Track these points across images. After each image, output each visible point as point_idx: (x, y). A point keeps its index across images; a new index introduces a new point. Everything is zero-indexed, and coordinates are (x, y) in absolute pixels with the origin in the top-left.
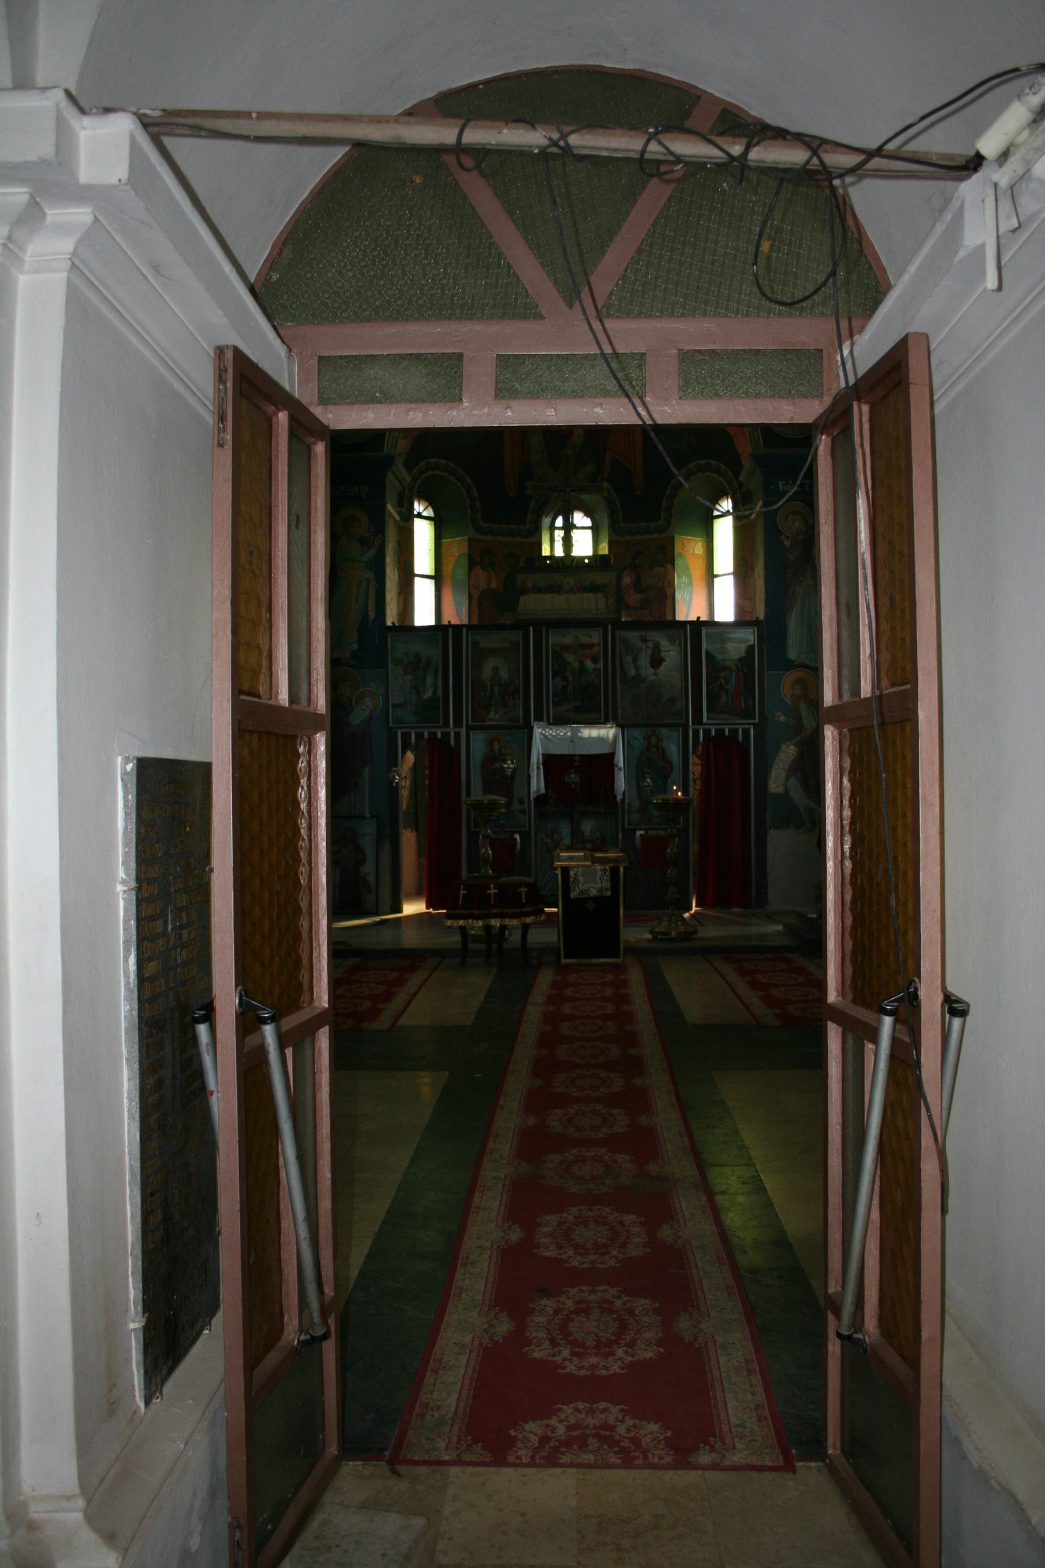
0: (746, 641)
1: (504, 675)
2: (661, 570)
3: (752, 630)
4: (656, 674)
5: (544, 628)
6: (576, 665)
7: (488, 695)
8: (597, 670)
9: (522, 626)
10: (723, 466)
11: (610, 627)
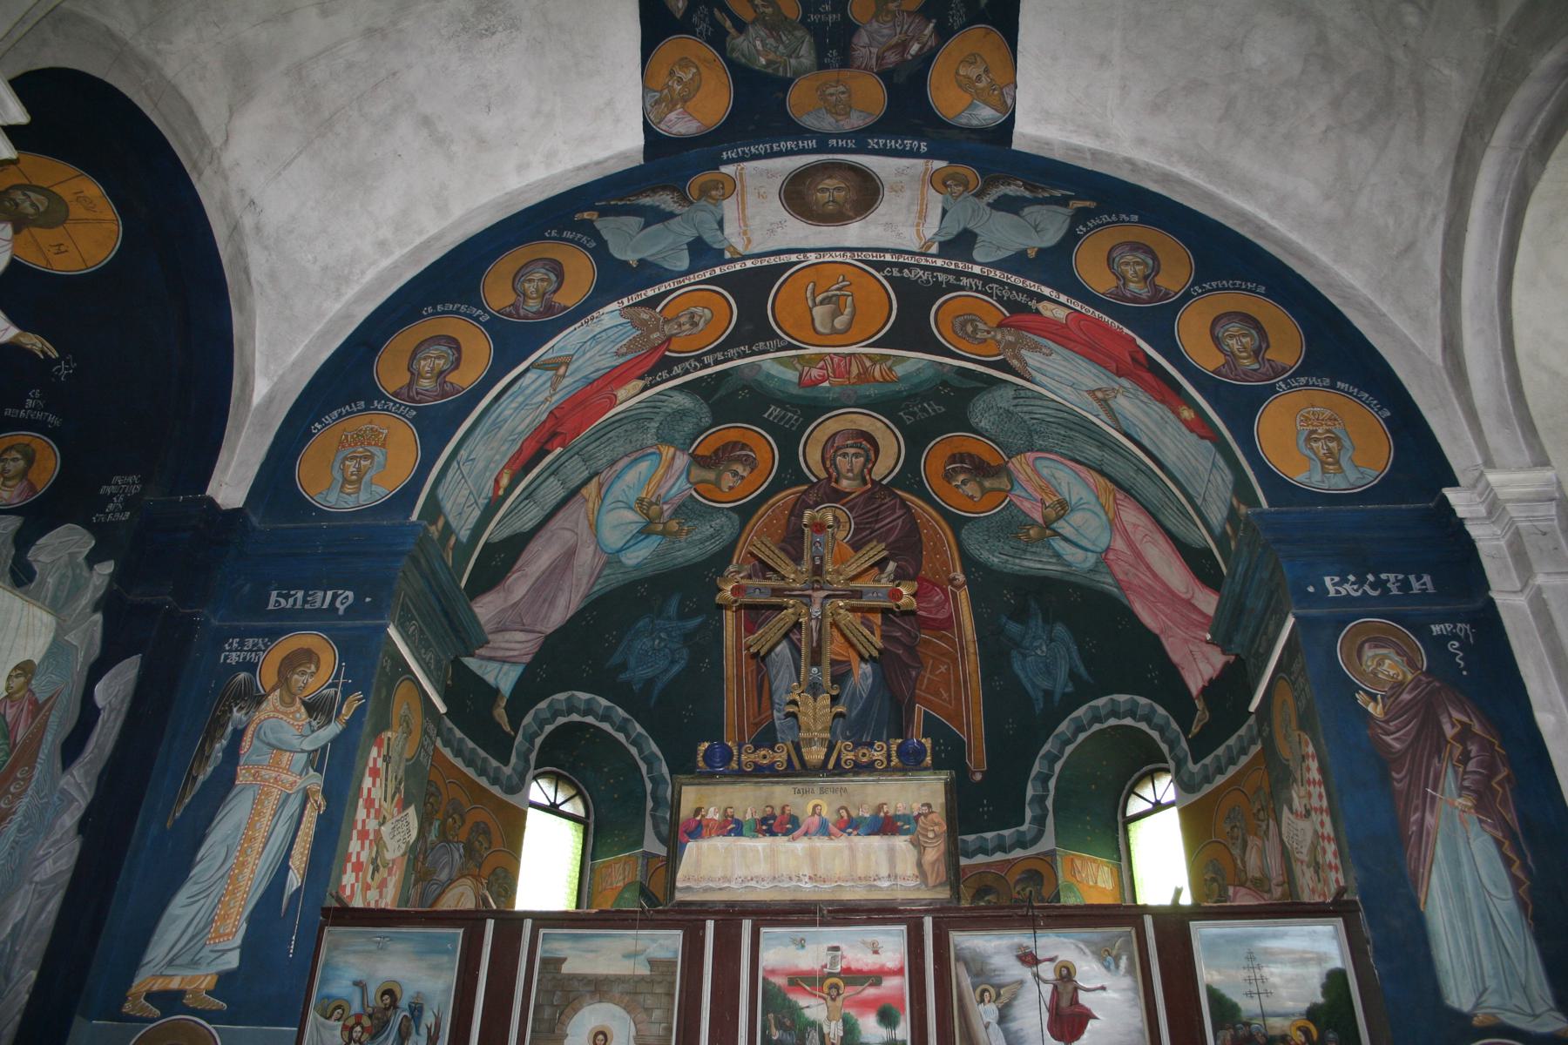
0: (1320, 959)
3: (1330, 928)
5: (747, 924)
6: (835, 1030)
9: (689, 918)
11: (928, 922)
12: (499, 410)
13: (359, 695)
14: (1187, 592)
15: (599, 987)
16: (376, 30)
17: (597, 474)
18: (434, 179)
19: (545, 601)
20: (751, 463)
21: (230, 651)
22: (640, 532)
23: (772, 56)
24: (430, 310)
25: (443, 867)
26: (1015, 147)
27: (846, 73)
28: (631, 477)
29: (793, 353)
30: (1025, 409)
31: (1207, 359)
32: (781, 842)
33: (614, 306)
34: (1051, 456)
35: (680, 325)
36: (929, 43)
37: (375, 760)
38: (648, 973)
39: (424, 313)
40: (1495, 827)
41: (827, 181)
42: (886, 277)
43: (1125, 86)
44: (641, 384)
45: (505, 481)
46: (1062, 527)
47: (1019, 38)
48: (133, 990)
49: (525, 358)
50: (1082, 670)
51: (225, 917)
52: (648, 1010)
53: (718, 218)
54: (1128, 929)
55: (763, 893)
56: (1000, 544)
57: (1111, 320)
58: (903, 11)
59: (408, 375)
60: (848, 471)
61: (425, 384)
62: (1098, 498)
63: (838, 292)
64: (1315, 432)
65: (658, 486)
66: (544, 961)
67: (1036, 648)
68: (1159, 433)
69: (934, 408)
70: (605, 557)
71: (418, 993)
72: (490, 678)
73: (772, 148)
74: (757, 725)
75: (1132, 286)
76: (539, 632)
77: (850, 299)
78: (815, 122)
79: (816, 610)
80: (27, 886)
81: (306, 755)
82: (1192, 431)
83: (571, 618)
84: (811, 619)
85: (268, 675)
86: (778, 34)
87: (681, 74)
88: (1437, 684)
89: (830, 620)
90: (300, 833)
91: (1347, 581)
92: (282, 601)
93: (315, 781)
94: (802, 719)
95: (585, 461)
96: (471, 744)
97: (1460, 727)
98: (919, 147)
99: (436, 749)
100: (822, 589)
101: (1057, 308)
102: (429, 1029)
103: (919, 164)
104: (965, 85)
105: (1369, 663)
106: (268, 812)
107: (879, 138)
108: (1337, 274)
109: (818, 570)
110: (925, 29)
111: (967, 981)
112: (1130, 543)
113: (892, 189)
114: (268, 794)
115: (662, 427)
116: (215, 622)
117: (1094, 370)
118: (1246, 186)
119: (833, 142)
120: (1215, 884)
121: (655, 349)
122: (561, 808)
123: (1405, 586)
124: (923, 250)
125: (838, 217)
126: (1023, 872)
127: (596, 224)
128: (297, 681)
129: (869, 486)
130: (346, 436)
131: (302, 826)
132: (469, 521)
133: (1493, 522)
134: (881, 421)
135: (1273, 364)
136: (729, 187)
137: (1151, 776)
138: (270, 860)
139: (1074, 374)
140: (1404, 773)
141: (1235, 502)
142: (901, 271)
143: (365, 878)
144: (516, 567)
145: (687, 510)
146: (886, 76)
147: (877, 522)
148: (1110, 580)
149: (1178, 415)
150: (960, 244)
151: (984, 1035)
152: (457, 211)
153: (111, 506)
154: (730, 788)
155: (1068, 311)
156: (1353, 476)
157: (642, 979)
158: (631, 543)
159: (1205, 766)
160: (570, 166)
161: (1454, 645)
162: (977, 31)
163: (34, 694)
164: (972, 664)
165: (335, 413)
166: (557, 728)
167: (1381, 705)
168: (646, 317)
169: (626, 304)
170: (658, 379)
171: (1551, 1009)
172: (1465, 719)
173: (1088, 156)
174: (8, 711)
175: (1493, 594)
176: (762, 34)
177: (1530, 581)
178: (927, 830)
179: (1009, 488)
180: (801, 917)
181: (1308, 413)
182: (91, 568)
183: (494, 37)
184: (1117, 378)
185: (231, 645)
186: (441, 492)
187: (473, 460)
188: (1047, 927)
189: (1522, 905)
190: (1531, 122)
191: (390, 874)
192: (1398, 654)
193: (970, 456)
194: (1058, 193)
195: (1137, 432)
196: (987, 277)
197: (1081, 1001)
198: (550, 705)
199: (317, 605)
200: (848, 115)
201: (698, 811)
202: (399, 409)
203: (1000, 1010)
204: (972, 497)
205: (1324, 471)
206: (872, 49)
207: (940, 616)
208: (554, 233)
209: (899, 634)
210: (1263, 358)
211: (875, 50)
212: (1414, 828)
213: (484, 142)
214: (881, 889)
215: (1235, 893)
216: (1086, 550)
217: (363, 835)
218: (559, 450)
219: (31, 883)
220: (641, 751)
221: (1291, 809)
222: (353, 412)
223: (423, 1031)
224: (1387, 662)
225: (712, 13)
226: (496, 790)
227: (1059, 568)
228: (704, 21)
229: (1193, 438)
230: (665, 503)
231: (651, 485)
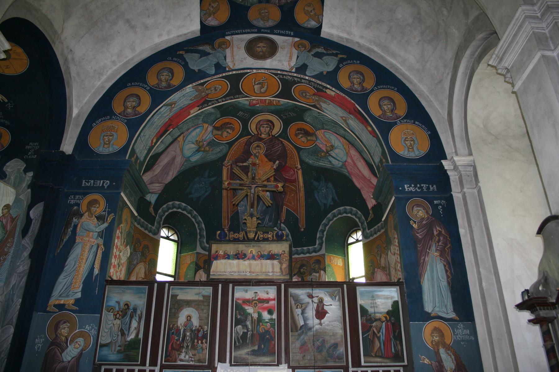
0: (392, 298)
1: (196, 322)
2: (317, 275)
3: (395, 289)
4: (321, 324)
5: (231, 285)
6: (255, 316)
7: (181, 339)
8: (271, 319)
9: (213, 283)
10: (354, 209)
11: (283, 285)
13: (113, 214)
14: (369, 177)
15: (188, 303)
17: (183, 133)
19: (165, 173)
20: (233, 129)
22: (196, 151)
24: (130, 84)
25: (135, 260)
26: (322, 36)
28: (194, 134)
29: (248, 98)
30: (321, 117)
31: (376, 112)
32: (241, 261)
33: (190, 86)
34: (329, 132)
35: (211, 91)
37: (118, 234)
38: (202, 299)
40: (444, 261)
41: (260, 44)
42: (278, 78)
44: (198, 108)
45: (155, 141)
46: (332, 153)
48: (49, 304)
49: (162, 103)
50: (336, 198)
51: (76, 283)
52: (203, 310)
53: (224, 55)
54: (339, 288)
55: (236, 276)
60: (264, 132)
61: (129, 111)
62: (343, 146)
64: (407, 138)
65: (203, 136)
66: (172, 296)
67: (323, 190)
69: (292, 114)
70: (185, 159)
71: (135, 305)
73: (242, 31)
74: (233, 211)
76: (164, 183)
77: (266, 83)
78: (257, 23)
79: (253, 191)
80: (15, 274)
81: (97, 233)
82: (371, 134)
84: (251, 194)
85: (84, 207)
87: (213, 5)
88: (434, 219)
89: (257, 194)
90: (97, 257)
93: (101, 241)
94: (248, 225)
95: (179, 129)
96: (142, 220)
97: (438, 232)
98: (291, 33)
99: (135, 226)
100: (254, 184)
101: (332, 92)
102: (139, 315)
103: (290, 39)
105: (415, 212)
106: (87, 251)
107: (278, 30)
108: (419, 87)
109: (253, 178)
111: (293, 302)
113: (281, 48)
114: (86, 245)
116: (66, 190)
118: (394, 55)
119: (263, 30)
120: (372, 267)
121: (203, 98)
122: (170, 238)
123: (428, 188)
124: (290, 70)
125: (263, 57)
126: (315, 260)
127: (184, 56)
128: (93, 210)
129: (271, 137)
130: (104, 128)
131: (98, 255)
136: (228, 44)
137: (356, 231)
138: (88, 265)
140: (421, 245)
141: (382, 158)
142: (283, 76)
143: (116, 269)
144: (156, 163)
145: (212, 144)
146: (281, 7)
147: (273, 148)
148: (346, 171)
149: (367, 129)
150: (302, 69)
151: (297, 317)
152: (138, 50)
153: (30, 153)
154: (226, 245)
155: (335, 93)
156: (417, 153)
157: (201, 301)
159: (371, 231)
160: (175, 35)
163: (11, 215)
164: (302, 194)
165: (100, 120)
166: (169, 213)
168: (200, 88)
171: (452, 312)
172: (440, 230)
173: (345, 40)
174: (4, 220)
175: (452, 193)
178: (283, 258)
180: (247, 283)
182: (25, 174)
184: (349, 114)
185: (71, 197)
186: (135, 147)
187: (145, 136)
188: (317, 287)
189: (449, 283)
190: (476, 51)
191: (123, 267)
192: (424, 209)
194: (334, 52)
196: (310, 80)
197: (325, 308)
198: (167, 206)
199: (98, 185)
200: (268, 21)
201: (217, 252)
202: (121, 119)
203: (302, 311)
204: (304, 142)
205: (408, 151)
207: (292, 178)
208: (170, 58)
210: (394, 113)
212: (422, 261)
214: (269, 275)
215: (377, 270)
216: (339, 161)
217: (115, 257)
219: (16, 273)
220: (196, 220)
221: (391, 252)
223: (137, 315)
224: (420, 211)
226: (150, 234)
227: (330, 166)
229: (371, 136)
230: (205, 142)
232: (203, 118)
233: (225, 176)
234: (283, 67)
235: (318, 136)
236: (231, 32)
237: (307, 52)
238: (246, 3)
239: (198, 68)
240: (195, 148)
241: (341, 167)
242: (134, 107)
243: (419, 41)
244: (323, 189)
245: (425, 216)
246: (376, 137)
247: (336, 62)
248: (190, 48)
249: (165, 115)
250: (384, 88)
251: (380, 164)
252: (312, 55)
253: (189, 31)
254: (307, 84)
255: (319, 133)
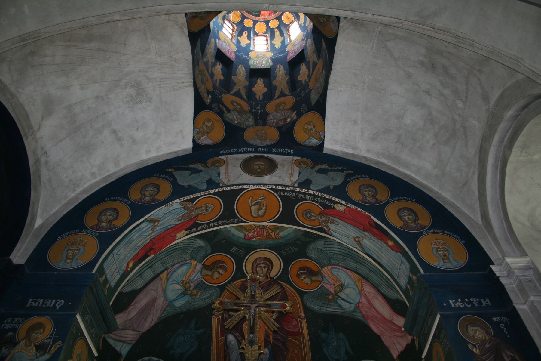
12: (131, 236)
13: (60, 342)
14: (390, 318)
16: (100, 97)
17: (167, 269)
18: (115, 153)
19: (142, 319)
20: (225, 269)
21: (7, 323)
22: (182, 294)
23: (239, 121)
24: (108, 199)
26: (324, 152)
27: (265, 128)
28: (180, 271)
30: (328, 249)
33: (178, 200)
34: (337, 267)
35: (202, 210)
36: (294, 118)
39: (106, 200)
41: (258, 162)
42: (278, 195)
43: (363, 131)
44: (186, 232)
45: (131, 265)
46: (342, 295)
47: (326, 114)
53: (218, 172)
56: (318, 302)
57: (361, 210)
58: (285, 109)
59: (98, 221)
61: (104, 224)
62: (355, 282)
63: (261, 201)
64: (439, 248)
65: (190, 276)
68: (380, 252)
72: (118, 349)
73: (238, 150)
75: (368, 198)
76: (140, 331)
79: (252, 312)
82: (393, 250)
83: (152, 327)
84: (250, 315)
86: (241, 114)
87: (207, 124)
91: (458, 301)
92: (33, 303)
98: (291, 152)
100: (255, 303)
101: (341, 206)
104: (307, 132)
105: (471, 333)
110: (292, 114)
112: (368, 300)
113: (281, 165)
115: (192, 253)
117: (355, 230)
118: (407, 165)
119: (260, 149)
121: (192, 219)
123: (480, 303)
124: (292, 185)
125: (262, 173)
129: (269, 279)
132: (115, 279)
133: (509, 278)
134: (274, 254)
135: (421, 225)
136: (222, 163)
139: (347, 232)
142: (284, 193)
144: (132, 304)
145: (200, 286)
146: (279, 128)
148: (360, 315)
149: (387, 244)
150: (306, 184)
152: (122, 165)
156: (455, 264)
158: (178, 298)
160: (165, 153)
161: (502, 326)
162: (311, 114)
164: (308, 349)
165: (67, 233)
167: (478, 349)
168: (189, 206)
169: (182, 200)
170: (192, 231)
172: (512, 355)
175: (515, 305)
176: (236, 114)
177: (528, 299)
179: (321, 280)
181: (436, 241)
183: (142, 104)
184: (363, 232)
186: (105, 265)
187: (119, 254)
192: (482, 329)
193: (307, 267)
194: (340, 168)
195: (371, 253)
196: (316, 195)
199: (48, 305)
200: (265, 140)
202: (92, 233)
204: (307, 284)
205: (444, 262)
206: (274, 120)
208: (157, 175)
209: (279, 338)
210: (417, 223)
211: (275, 121)
213: (135, 141)
216: (351, 303)
218: (153, 255)
222: (74, 233)
225: (219, 105)
227: (341, 311)
228: (216, 107)
229: (393, 252)
230: (192, 283)
231: (187, 276)
232: (191, 253)
233: (214, 328)
234: (284, 182)
235: (324, 274)
236: (226, 152)
237: (309, 169)
238: (242, 125)
239: (189, 184)
240: (181, 290)
241: (354, 311)
242: (110, 221)
243: (433, 145)
244: (332, 341)
245: (486, 338)
246: (400, 252)
247: (342, 177)
248: (180, 166)
249: (145, 235)
250: (401, 200)
251: (408, 286)
252: (315, 171)
253: (180, 149)
254: (312, 201)
255: (325, 271)
